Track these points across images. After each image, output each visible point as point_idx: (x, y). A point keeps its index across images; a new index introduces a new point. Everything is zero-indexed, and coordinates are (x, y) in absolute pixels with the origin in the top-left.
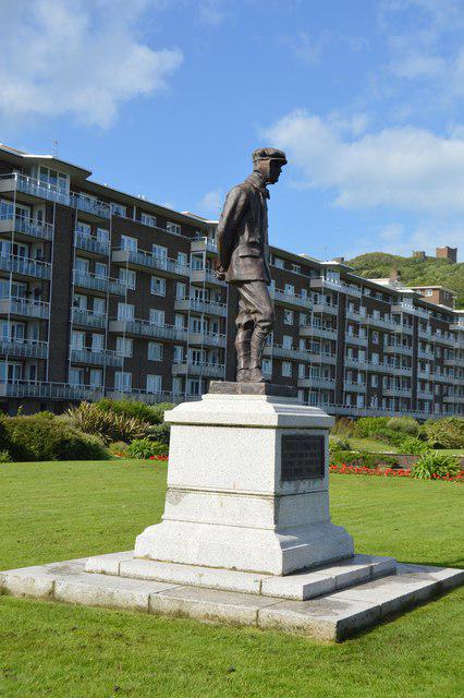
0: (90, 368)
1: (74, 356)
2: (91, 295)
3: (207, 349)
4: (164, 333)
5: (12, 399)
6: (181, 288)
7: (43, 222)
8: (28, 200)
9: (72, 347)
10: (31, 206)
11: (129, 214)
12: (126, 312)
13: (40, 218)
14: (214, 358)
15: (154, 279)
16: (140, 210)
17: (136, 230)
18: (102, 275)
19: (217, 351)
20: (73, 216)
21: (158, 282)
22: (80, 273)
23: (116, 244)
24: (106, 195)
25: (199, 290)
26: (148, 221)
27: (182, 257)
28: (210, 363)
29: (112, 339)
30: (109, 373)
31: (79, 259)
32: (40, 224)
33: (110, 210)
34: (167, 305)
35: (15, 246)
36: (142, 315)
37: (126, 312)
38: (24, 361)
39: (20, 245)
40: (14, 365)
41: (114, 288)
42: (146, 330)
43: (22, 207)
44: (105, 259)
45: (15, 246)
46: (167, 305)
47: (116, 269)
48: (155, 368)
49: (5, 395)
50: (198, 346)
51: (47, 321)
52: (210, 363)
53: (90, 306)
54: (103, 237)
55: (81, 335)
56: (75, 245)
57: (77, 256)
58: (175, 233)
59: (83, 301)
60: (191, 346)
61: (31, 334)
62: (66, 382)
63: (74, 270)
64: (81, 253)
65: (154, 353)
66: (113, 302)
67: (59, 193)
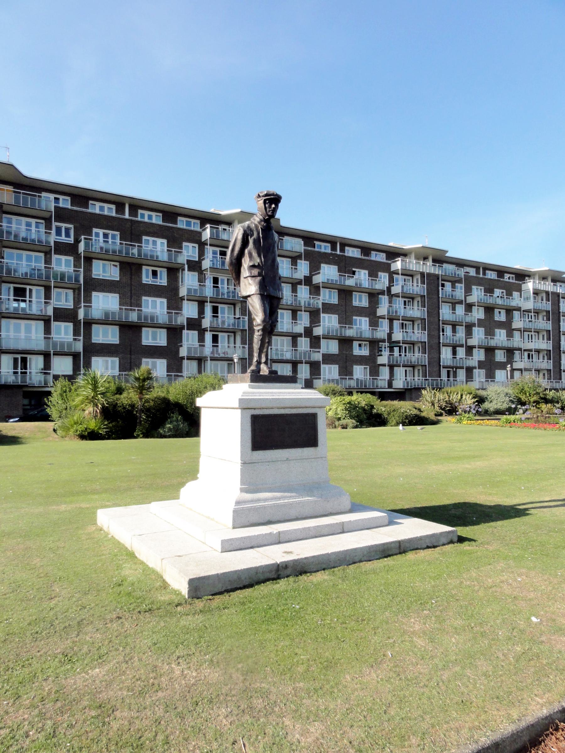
0: (456, 369)
1: (443, 363)
2: (454, 326)
3: (538, 351)
4: (506, 344)
5: (406, 389)
6: (516, 314)
7: (419, 284)
8: (409, 273)
9: (443, 356)
10: (412, 276)
11: (478, 272)
12: (478, 335)
13: (417, 283)
14: (544, 357)
15: (496, 311)
16: (485, 269)
17: (479, 282)
18: (460, 310)
19: (546, 352)
20: (438, 279)
21: (500, 312)
22: (445, 312)
23: (468, 291)
24: (460, 264)
25: (530, 334)
26: (491, 275)
27: (516, 294)
28: (541, 360)
29: (470, 350)
30: (469, 371)
31: (443, 303)
32: (417, 286)
33: (461, 272)
34: (507, 325)
35: (402, 324)
36: (490, 333)
37: (478, 335)
38: (413, 367)
39: (405, 322)
40: (408, 369)
41: (468, 319)
42: (492, 343)
43: (407, 278)
44: (460, 302)
45: (402, 324)
46: (507, 325)
47: (469, 307)
48: (501, 325)
49: (402, 387)
50: (531, 350)
51: (425, 342)
52: (541, 360)
53: (454, 331)
54: (460, 289)
55: (449, 349)
56: (440, 296)
57: (442, 302)
58: (511, 281)
59: (449, 329)
60: (525, 350)
61: (416, 326)
62: (440, 377)
63: (440, 311)
64: (445, 300)
65: (500, 356)
66: (469, 328)
67: (429, 267)
